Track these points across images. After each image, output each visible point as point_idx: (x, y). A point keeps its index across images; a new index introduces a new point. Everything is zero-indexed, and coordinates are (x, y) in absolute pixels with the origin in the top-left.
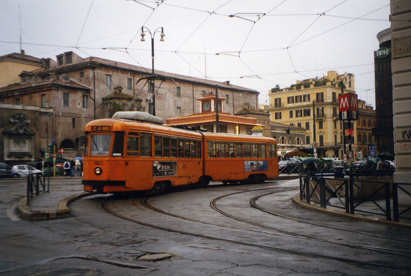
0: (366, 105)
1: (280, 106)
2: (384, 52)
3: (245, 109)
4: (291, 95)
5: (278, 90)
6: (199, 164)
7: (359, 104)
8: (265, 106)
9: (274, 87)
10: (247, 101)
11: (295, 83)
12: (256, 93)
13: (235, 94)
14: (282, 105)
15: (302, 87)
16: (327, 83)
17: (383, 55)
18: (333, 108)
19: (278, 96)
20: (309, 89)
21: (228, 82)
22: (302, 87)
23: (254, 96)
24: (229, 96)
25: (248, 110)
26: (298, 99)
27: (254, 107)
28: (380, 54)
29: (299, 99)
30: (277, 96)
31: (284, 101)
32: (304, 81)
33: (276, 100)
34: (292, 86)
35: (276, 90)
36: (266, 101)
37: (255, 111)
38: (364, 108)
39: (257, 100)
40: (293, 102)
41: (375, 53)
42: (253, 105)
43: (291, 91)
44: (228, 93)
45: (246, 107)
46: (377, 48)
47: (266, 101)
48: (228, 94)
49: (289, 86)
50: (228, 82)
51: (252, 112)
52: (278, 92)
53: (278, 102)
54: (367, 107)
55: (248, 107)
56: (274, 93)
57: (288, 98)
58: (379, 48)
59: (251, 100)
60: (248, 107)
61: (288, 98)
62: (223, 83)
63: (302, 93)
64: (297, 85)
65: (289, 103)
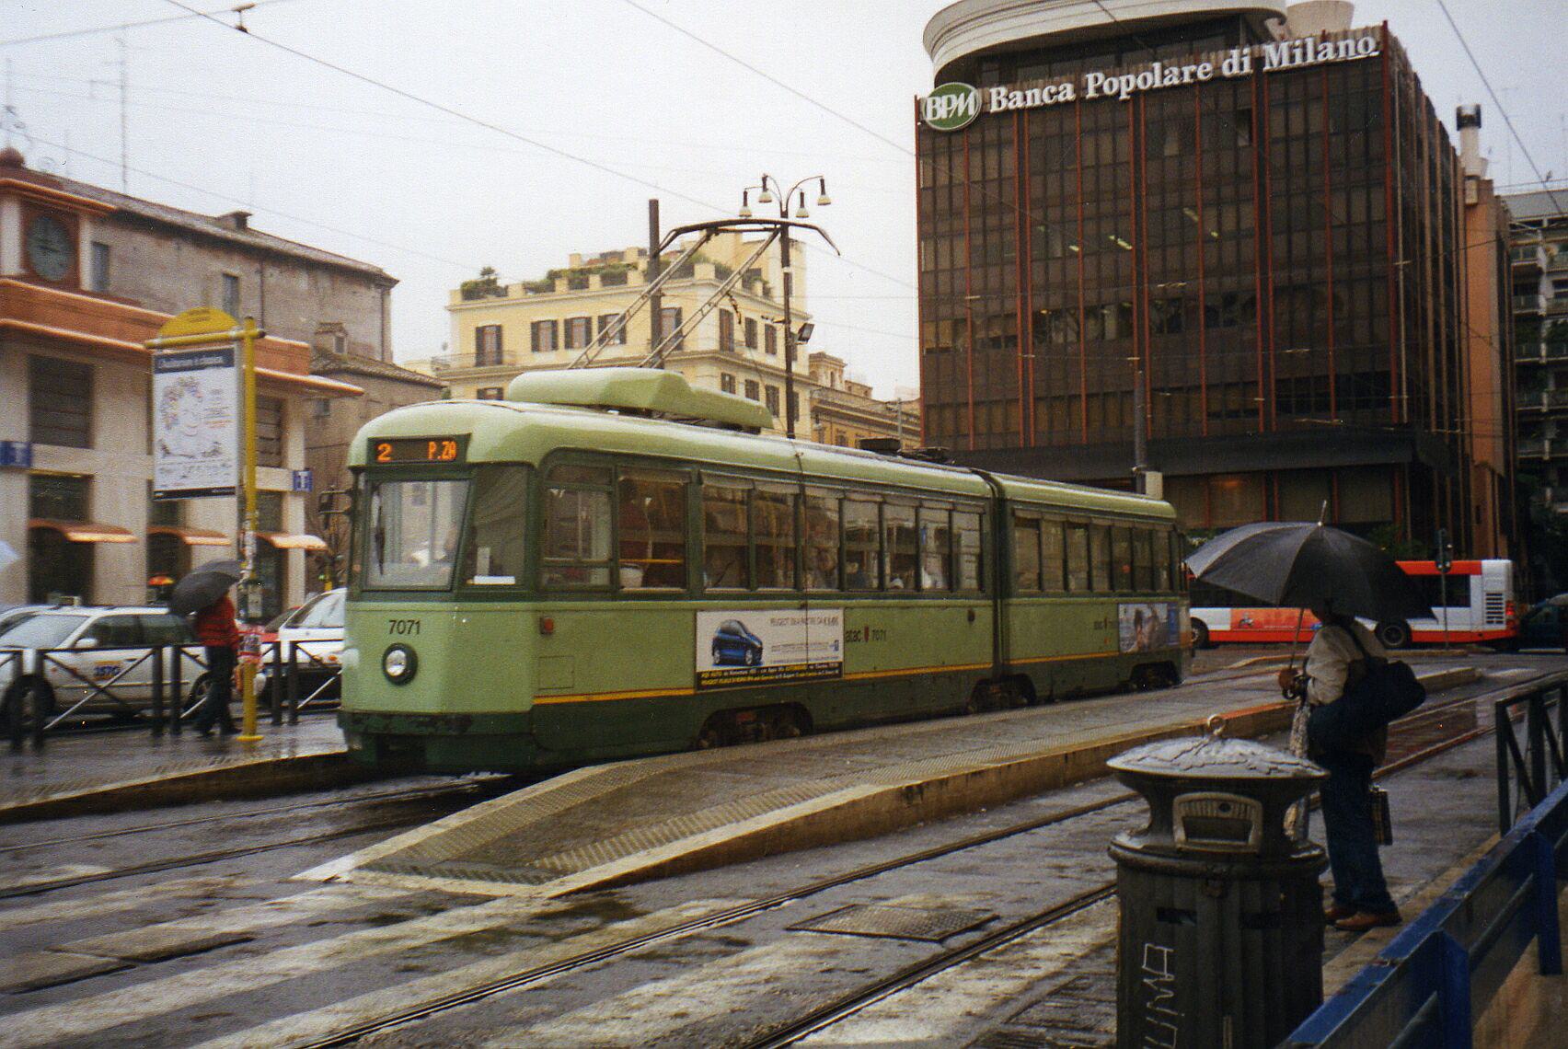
0: (846, 377)
1: (500, 362)
2: (959, 103)
3: (323, 353)
4: (545, 313)
5: (487, 292)
6: (971, 617)
7: (821, 371)
8: (434, 361)
9: (474, 276)
10: (332, 315)
11: (563, 264)
12: (380, 282)
13: (274, 276)
14: (507, 358)
15: (595, 281)
16: (698, 268)
17: (954, 117)
18: (723, 375)
19: (488, 318)
20: (622, 289)
21: (240, 219)
22: (595, 281)
23: (369, 296)
24: (243, 284)
25: (335, 359)
26: (572, 333)
27: (369, 348)
28: (942, 113)
29: (579, 333)
30: (487, 315)
31: (516, 341)
32: (604, 256)
33: (480, 332)
34: (554, 275)
35: (481, 290)
36: (445, 347)
37: (371, 361)
38: (839, 386)
39: (384, 312)
40: (555, 347)
41: (918, 104)
42: (361, 331)
43: (548, 296)
44: (236, 267)
45: (330, 342)
46: (926, 87)
47: (445, 347)
48: (235, 271)
49: (539, 276)
50: (240, 219)
51: (352, 365)
52: (491, 298)
53: (488, 344)
54: (850, 385)
55: (340, 340)
56: (472, 304)
57: (536, 327)
58: (931, 89)
59: (353, 307)
60: (340, 340)
61: (536, 327)
62: (218, 221)
63: (596, 303)
64: (573, 271)
65: (536, 348)
